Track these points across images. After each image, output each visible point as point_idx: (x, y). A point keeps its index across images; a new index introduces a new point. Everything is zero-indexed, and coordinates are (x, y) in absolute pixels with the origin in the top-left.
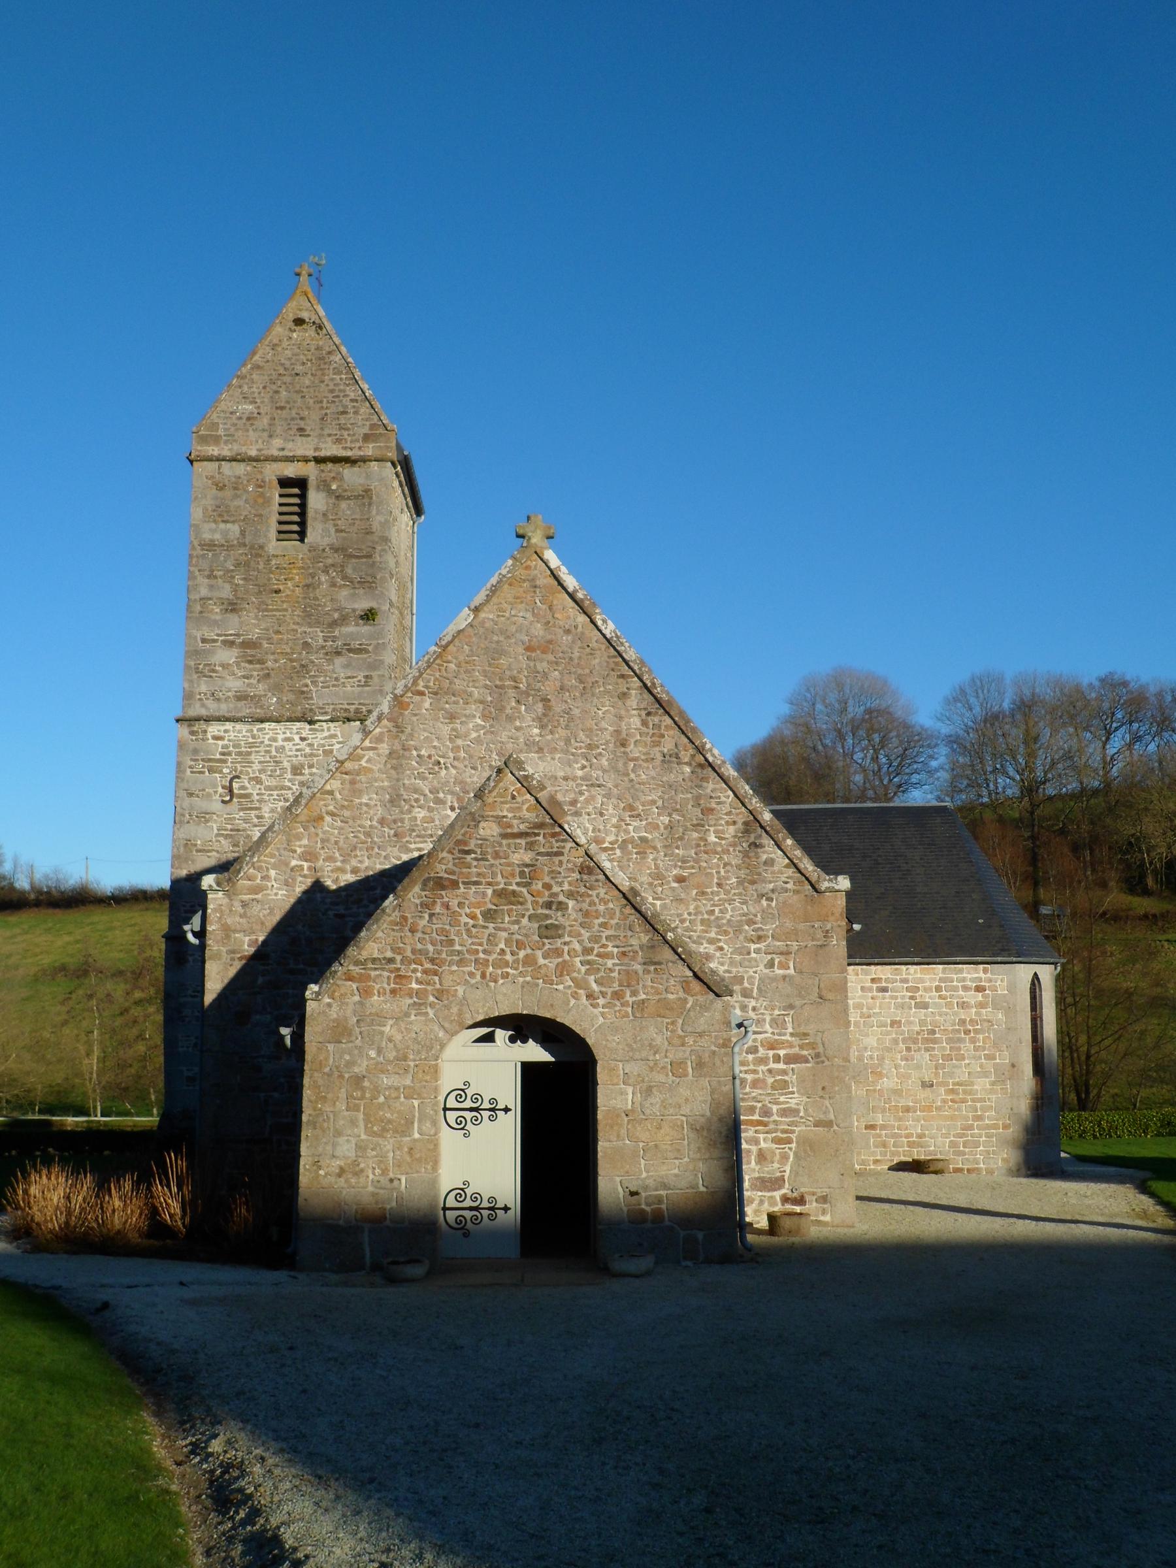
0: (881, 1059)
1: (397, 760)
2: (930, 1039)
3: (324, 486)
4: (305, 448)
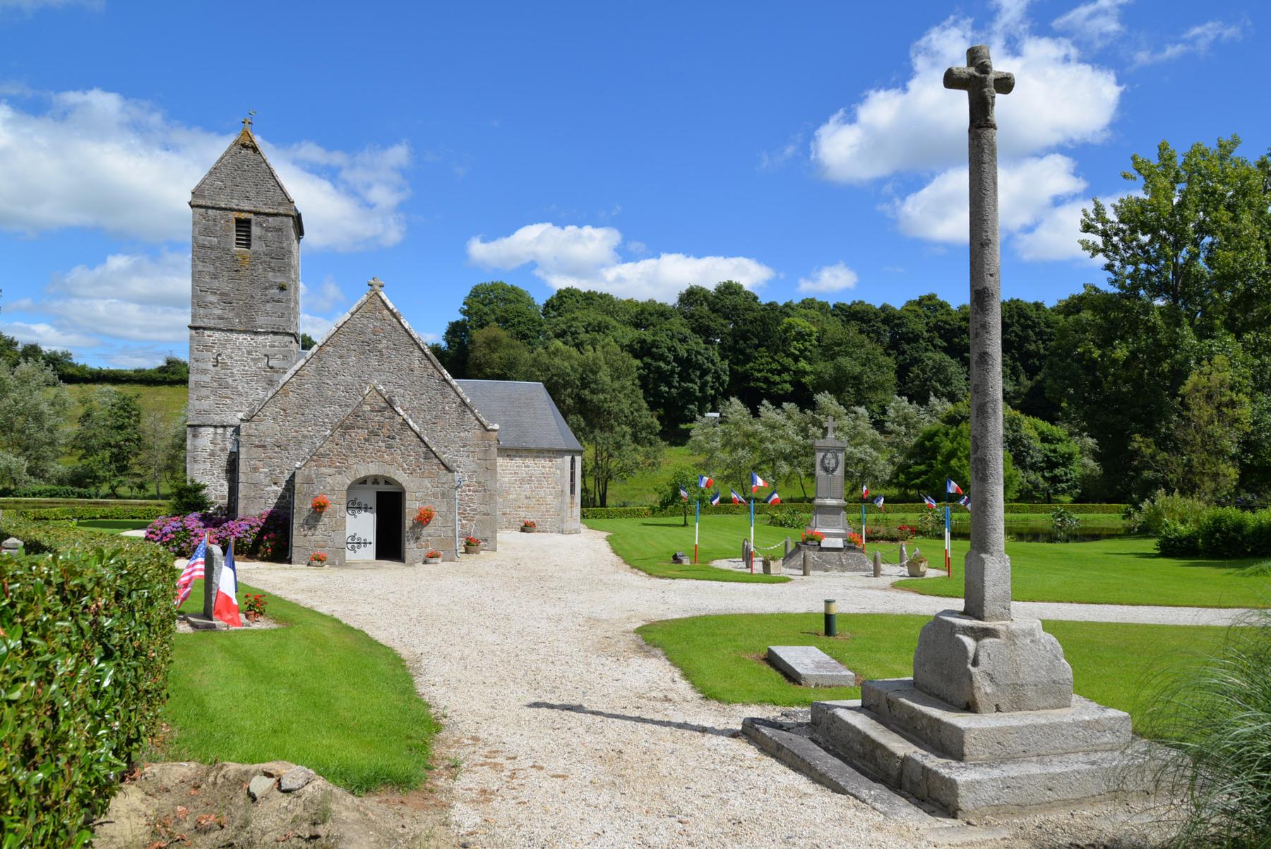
1: (319, 372)
2: (530, 480)
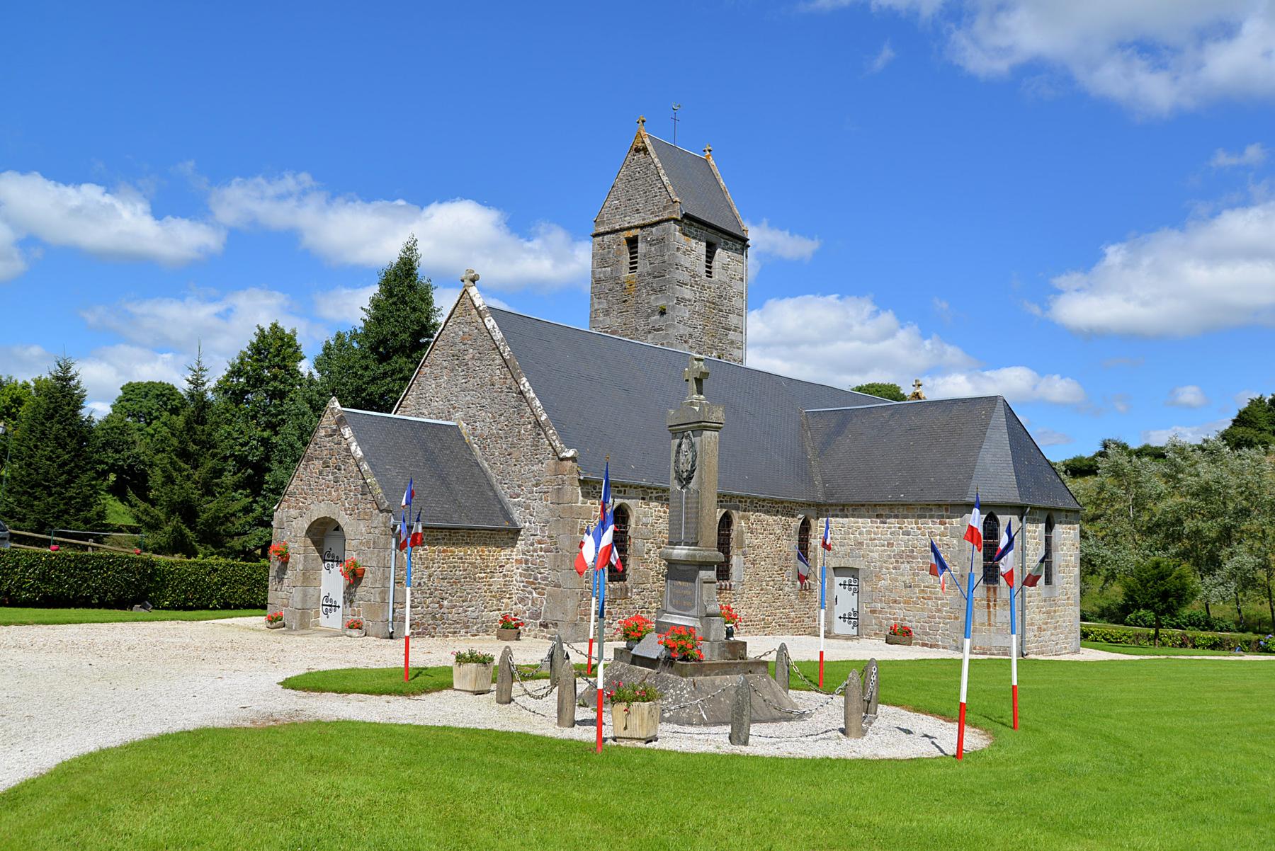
0: (881, 568)
3: (645, 238)
4: (637, 221)
